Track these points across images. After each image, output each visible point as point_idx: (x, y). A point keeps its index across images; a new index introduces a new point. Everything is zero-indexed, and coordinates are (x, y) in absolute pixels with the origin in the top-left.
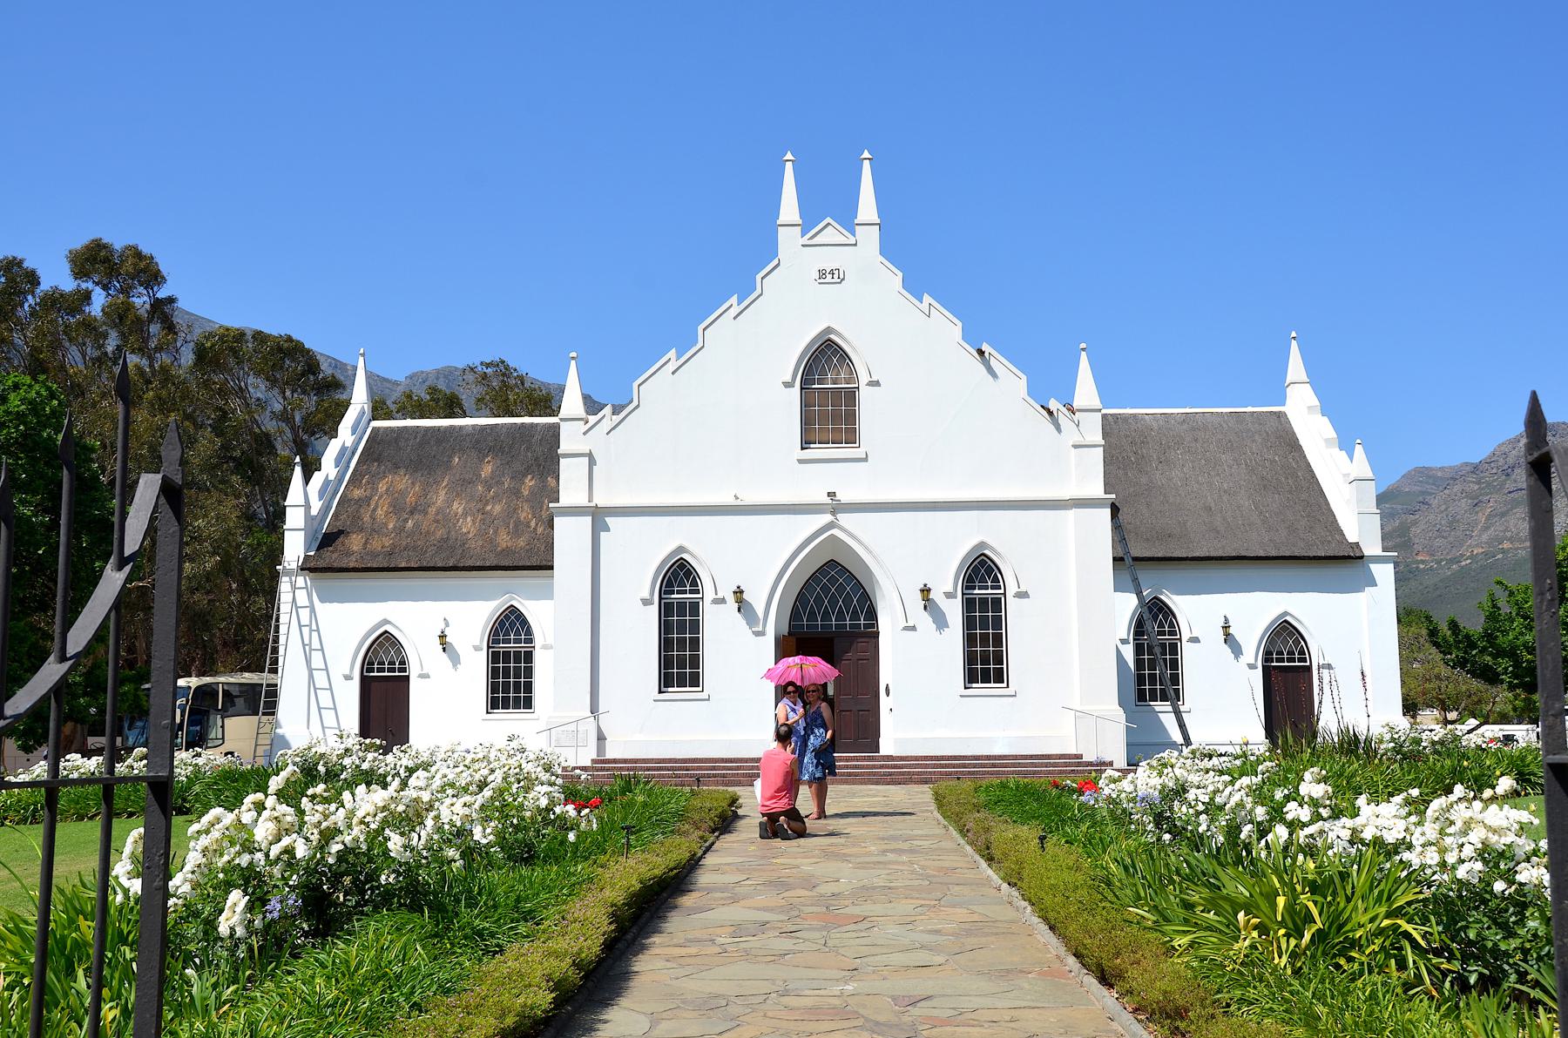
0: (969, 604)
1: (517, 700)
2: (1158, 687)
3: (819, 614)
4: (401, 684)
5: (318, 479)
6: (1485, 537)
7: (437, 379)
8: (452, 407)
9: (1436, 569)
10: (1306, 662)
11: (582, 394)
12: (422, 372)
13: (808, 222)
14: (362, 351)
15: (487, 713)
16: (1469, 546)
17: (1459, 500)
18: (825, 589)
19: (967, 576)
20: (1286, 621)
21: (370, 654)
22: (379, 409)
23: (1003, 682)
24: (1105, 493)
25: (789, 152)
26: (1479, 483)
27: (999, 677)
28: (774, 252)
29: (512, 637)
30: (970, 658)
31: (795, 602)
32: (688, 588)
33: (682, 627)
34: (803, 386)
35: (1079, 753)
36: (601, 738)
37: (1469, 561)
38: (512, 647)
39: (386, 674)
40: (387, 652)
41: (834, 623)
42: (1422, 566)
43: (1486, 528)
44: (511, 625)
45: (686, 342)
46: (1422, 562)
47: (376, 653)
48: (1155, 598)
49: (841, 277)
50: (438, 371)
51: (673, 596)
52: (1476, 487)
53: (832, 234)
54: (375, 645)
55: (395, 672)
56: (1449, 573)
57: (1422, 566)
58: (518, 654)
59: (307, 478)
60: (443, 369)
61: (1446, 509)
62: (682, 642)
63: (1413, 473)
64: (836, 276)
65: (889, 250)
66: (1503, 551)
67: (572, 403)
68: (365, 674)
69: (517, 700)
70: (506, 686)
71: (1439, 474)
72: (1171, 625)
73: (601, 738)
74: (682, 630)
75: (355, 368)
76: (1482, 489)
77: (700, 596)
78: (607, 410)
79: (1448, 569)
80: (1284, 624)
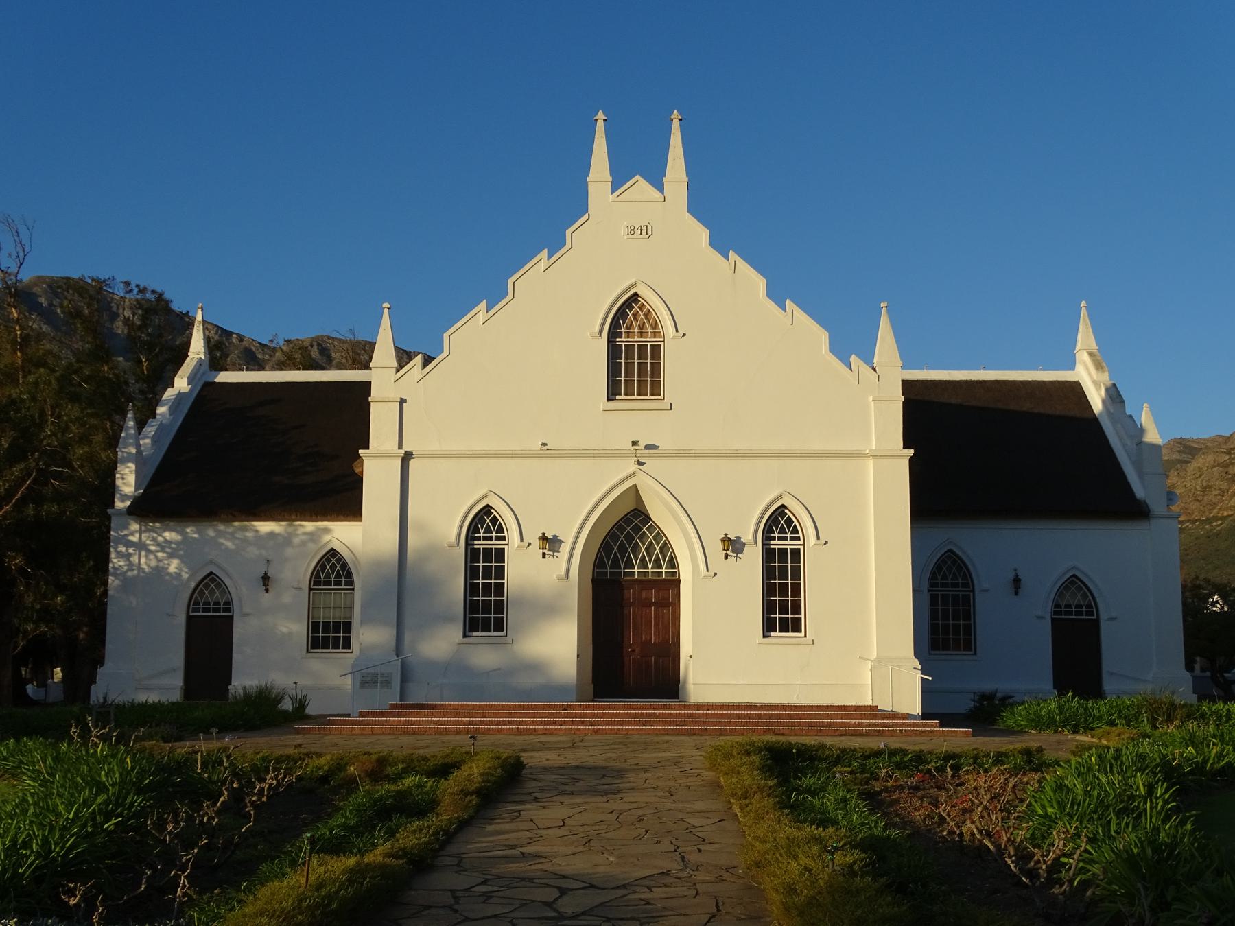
0: (768, 554)
1: (336, 640)
3: (608, 563)
4: (1092, 628)
5: (150, 430)
10: (1093, 615)
11: (395, 347)
14: (200, 305)
15: (308, 652)
16: (1220, 509)
17: (1212, 469)
19: (767, 527)
21: (196, 594)
23: (503, 631)
24: (904, 448)
25: (600, 111)
27: (797, 627)
28: (584, 210)
29: (333, 579)
30: (768, 607)
31: (599, 549)
32: (482, 535)
34: (610, 340)
35: (874, 704)
40: (212, 592)
41: (636, 570)
45: (495, 294)
48: (950, 551)
49: (650, 233)
50: (312, 339)
52: (1227, 457)
53: (640, 187)
54: (201, 586)
56: (1202, 533)
58: (955, 597)
60: (318, 337)
61: (1200, 476)
64: (644, 232)
65: (696, 207)
67: (384, 354)
68: (191, 614)
71: (1196, 446)
78: (419, 359)
80: (1073, 578)
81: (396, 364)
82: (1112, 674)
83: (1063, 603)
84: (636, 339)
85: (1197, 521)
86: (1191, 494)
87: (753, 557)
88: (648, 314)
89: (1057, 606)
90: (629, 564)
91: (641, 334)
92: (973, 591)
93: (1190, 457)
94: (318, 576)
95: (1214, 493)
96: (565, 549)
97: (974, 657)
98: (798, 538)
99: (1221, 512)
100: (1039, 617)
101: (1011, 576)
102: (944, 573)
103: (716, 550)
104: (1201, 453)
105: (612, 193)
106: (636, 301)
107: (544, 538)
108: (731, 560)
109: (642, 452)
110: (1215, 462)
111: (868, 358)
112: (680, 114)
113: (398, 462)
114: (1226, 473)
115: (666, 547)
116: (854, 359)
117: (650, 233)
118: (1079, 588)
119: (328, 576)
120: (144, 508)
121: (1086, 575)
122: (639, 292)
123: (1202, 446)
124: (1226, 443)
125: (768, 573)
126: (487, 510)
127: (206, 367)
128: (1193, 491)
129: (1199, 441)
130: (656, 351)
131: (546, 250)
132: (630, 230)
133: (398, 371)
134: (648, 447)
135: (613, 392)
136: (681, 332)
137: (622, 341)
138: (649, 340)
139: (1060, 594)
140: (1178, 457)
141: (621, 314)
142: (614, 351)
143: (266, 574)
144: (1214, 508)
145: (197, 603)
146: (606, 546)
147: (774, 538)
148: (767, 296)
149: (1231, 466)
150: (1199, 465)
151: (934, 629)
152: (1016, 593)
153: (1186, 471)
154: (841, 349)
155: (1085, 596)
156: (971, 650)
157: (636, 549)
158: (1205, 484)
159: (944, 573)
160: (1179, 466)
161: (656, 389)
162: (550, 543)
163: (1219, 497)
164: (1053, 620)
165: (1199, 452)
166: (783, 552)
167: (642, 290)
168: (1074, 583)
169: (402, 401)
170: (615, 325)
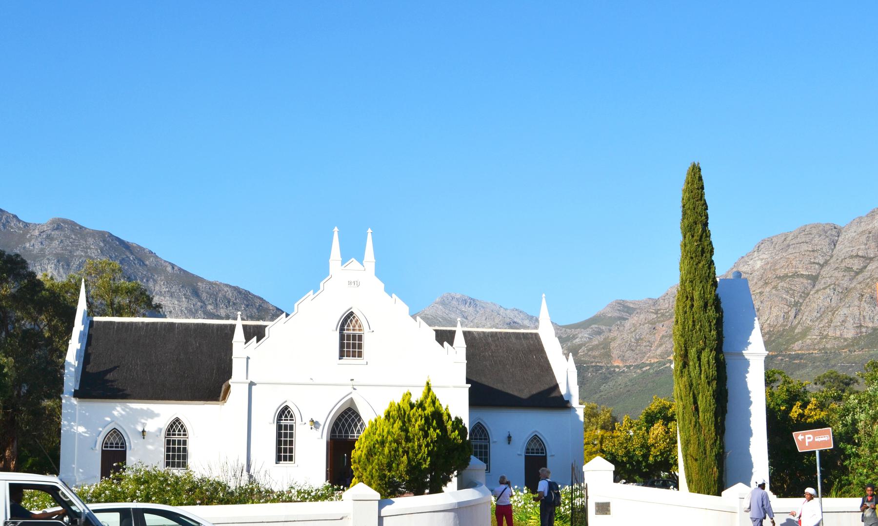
6: (659, 352)
9: (627, 372)
10: (544, 454)
13: (345, 259)
15: (276, 463)
16: (648, 357)
17: (644, 325)
18: (346, 420)
20: (536, 435)
26: (656, 313)
33: (286, 435)
37: (648, 368)
38: (176, 438)
39: (114, 449)
42: (617, 370)
43: (661, 345)
44: (176, 426)
46: (618, 367)
47: (109, 438)
48: (479, 423)
49: (358, 284)
51: (281, 422)
52: (655, 316)
53: (354, 264)
55: (529, 453)
56: (635, 376)
57: (617, 370)
61: (634, 331)
62: (286, 442)
63: (614, 304)
64: (356, 284)
65: (378, 274)
68: (104, 449)
70: (174, 456)
71: (631, 306)
72: (485, 436)
74: (286, 436)
76: (659, 318)
77: (294, 422)
79: (634, 372)
81: (245, 341)
85: (631, 366)
88: (357, 321)
89: (527, 449)
90: (353, 432)
92: (489, 442)
93: (628, 314)
94: (169, 431)
95: (644, 344)
96: (321, 428)
99: (649, 360)
100: (519, 455)
101: (507, 435)
104: (635, 312)
105: (342, 265)
110: (646, 320)
112: (338, 229)
113: (247, 385)
114: (654, 328)
116: (446, 344)
117: (358, 284)
118: (538, 441)
119: (174, 431)
122: (354, 311)
123: (637, 307)
124: (654, 305)
126: (286, 408)
128: (629, 342)
130: (360, 338)
131: (312, 291)
132: (350, 283)
133: (246, 343)
135: (341, 356)
139: (529, 444)
140: (618, 315)
143: (144, 430)
144: (644, 357)
145: (106, 443)
148: (376, 275)
149: (657, 323)
150: (634, 322)
152: (509, 443)
153: (624, 327)
155: (540, 445)
157: (356, 426)
158: (638, 337)
160: (619, 322)
161: (360, 355)
162: (315, 424)
163: (648, 348)
164: (525, 456)
165: (635, 310)
169: (248, 358)
170: (343, 325)
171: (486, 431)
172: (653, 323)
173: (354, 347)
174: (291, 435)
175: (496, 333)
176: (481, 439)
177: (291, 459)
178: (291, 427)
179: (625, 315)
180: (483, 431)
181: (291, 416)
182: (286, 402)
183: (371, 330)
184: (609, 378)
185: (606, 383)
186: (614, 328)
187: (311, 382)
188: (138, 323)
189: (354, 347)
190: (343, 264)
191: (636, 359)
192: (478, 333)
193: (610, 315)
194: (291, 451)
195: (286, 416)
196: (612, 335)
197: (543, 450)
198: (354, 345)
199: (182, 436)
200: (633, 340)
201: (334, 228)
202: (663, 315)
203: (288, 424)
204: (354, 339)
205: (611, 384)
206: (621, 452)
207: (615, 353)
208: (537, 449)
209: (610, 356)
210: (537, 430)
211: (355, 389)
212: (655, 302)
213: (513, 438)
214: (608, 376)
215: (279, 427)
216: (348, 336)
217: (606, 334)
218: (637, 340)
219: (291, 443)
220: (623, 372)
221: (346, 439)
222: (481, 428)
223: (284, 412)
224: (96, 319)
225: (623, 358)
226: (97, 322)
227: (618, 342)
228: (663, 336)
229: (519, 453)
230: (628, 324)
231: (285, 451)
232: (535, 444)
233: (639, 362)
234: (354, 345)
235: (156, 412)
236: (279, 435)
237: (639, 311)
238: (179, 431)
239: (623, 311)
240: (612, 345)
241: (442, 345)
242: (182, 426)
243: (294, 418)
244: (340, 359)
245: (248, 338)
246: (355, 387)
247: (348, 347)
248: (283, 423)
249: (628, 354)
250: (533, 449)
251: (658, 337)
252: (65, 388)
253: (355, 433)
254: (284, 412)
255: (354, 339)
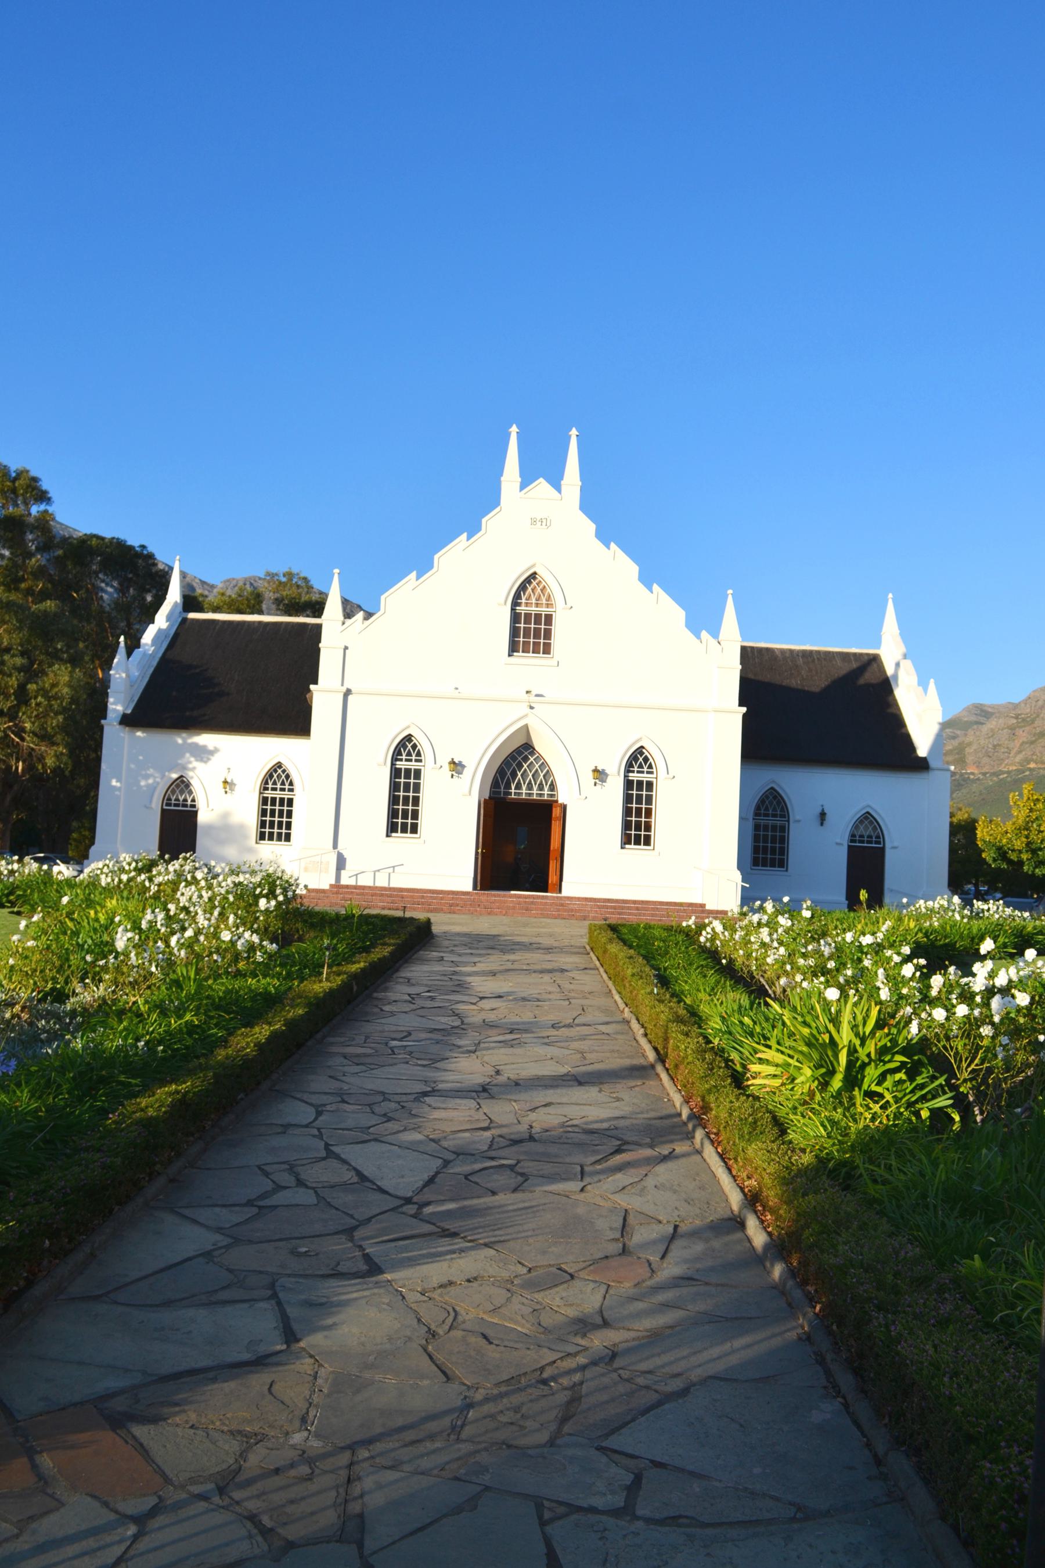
0: (629, 784)
1: (280, 835)
2: (769, 856)
6: (1018, 759)
7: (245, 584)
8: (255, 604)
9: (982, 779)
12: (234, 579)
16: (1007, 765)
20: (868, 813)
22: (190, 602)
26: (1017, 718)
27: (647, 841)
30: (627, 825)
36: (341, 863)
37: (1005, 775)
38: (278, 794)
43: (1020, 752)
45: (424, 567)
46: (972, 773)
49: (548, 524)
50: (246, 579)
53: (542, 486)
57: (972, 777)
58: (282, 800)
59: (129, 654)
60: (250, 578)
61: (992, 736)
64: (544, 524)
65: (586, 506)
66: (1030, 769)
67: (333, 608)
68: (165, 807)
69: (280, 835)
71: (990, 710)
72: (782, 810)
73: (341, 863)
75: (171, 569)
77: (654, 776)
78: (360, 615)
82: (892, 891)
83: (857, 834)
84: (534, 609)
85: (987, 773)
86: (984, 751)
87: (615, 786)
88: (543, 589)
89: (853, 835)
91: (537, 605)
92: (788, 821)
95: (1003, 750)
96: (467, 773)
97: (785, 873)
98: (652, 773)
101: (819, 810)
102: (767, 806)
103: (588, 778)
105: (521, 491)
106: (535, 578)
107: (453, 762)
108: (598, 787)
109: (532, 698)
111: (715, 634)
112: (578, 431)
113: (341, 695)
115: (548, 774)
116: (704, 634)
118: (871, 823)
120: (127, 721)
121: (876, 811)
122: (538, 572)
125: (628, 799)
126: (409, 738)
127: (180, 608)
129: (992, 707)
130: (549, 619)
132: (534, 522)
134: (537, 695)
135: (513, 648)
136: (569, 605)
137: (522, 609)
138: (544, 610)
139: (856, 826)
141: (523, 587)
142: (515, 618)
143: (823, 810)
144: (1001, 764)
146: (501, 772)
147: (633, 772)
148: (581, 508)
151: (756, 850)
152: (822, 824)
154: (695, 625)
155: (875, 829)
156: (783, 867)
159: (767, 806)
162: (456, 767)
164: (849, 847)
166: (640, 783)
167: (541, 572)
168: (868, 818)
169: (346, 648)
170: (517, 596)
171: (784, 801)
172: (1012, 728)
173: (537, 635)
174: (417, 788)
175: (811, 652)
176: (775, 816)
177: (414, 829)
178: (418, 774)
179: (982, 719)
180: (779, 803)
181: (419, 754)
182: (408, 727)
183: (569, 606)
184: (962, 785)
185: (959, 790)
186: (971, 732)
187: (455, 693)
188: (254, 622)
189: (537, 635)
190: (522, 488)
191: (994, 766)
192: (782, 651)
193: (966, 719)
194: (415, 815)
195: (409, 754)
196: (967, 740)
197: (880, 838)
198: (537, 632)
199: (286, 792)
200: (990, 746)
201: (511, 427)
202: (1024, 720)
203: (413, 767)
204: (538, 621)
205: (964, 791)
206: (1019, 844)
207: (970, 759)
208: (870, 837)
209: (964, 762)
210: (871, 804)
211: (532, 708)
212: (1016, 706)
213: (828, 817)
214: (962, 782)
215: (395, 773)
216: (528, 616)
217: (960, 739)
218: (995, 746)
219: (416, 801)
220: (978, 779)
221: (505, 799)
222: (775, 797)
223: (406, 747)
224: (192, 615)
225: (978, 763)
226: (193, 620)
227: (974, 747)
228: (1023, 742)
229: (838, 841)
230: (985, 729)
231: (405, 815)
232: (866, 828)
233: (996, 769)
234: (537, 632)
235: (211, 747)
236: (394, 787)
237: (997, 715)
238: (283, 784)
239: (981, 715)
240: (967, 750)
241: (698, 637)
242: (288, 776)
243: (423, 758)
244: (509, 655)
245: (348, 614)
246: (532, 705)
247: (527, 634)
248: (402, 765)
249: (985, 760)
250: (861, 836)
251: (1017, 743)
252: (111, 715)
253: (513, 788)
254: (406, 747)
255: (538, 621)
